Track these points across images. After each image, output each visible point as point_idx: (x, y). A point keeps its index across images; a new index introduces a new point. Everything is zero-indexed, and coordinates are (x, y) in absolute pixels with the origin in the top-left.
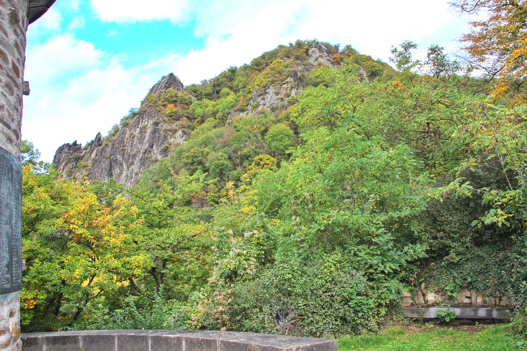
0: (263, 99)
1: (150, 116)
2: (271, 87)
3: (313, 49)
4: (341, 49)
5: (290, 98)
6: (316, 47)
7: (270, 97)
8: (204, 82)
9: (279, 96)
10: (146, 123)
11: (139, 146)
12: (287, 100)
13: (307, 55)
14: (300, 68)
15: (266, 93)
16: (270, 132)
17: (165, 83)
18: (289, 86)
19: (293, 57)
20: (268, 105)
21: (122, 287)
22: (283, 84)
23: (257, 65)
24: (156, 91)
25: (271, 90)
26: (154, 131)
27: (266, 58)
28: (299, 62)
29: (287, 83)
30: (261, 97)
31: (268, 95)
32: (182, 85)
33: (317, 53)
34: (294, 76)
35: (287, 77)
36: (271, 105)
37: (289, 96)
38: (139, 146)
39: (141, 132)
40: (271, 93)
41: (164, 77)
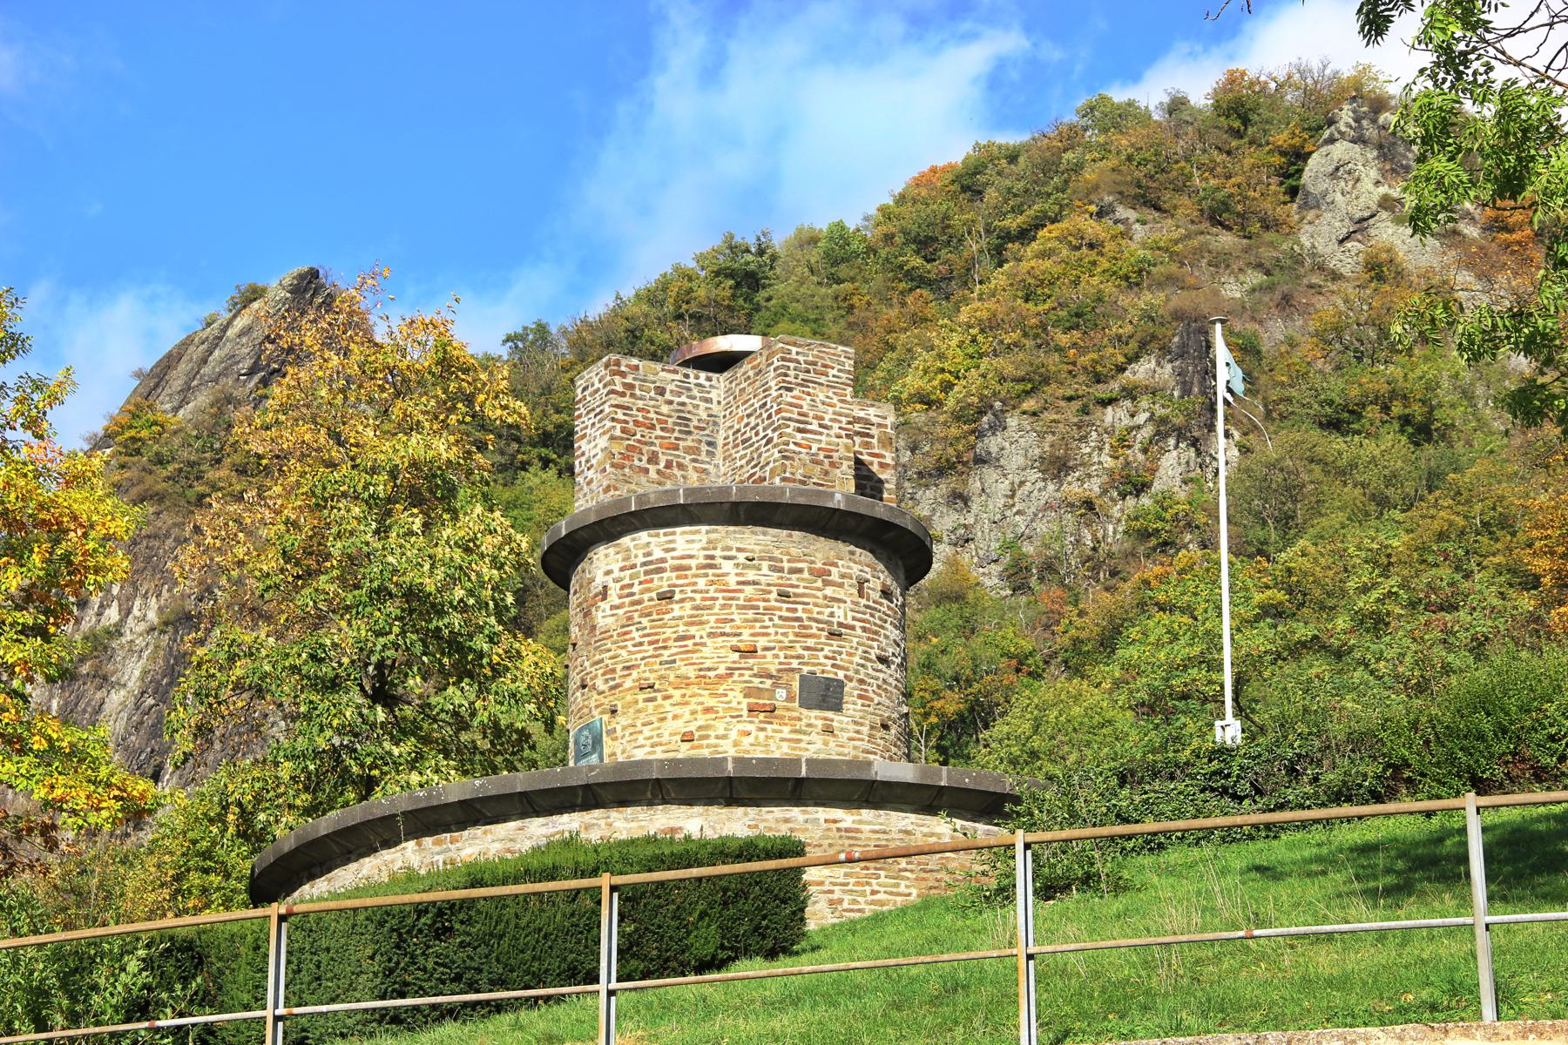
0: (960, 499)
2: (1012, 421)
3: (1341, 150)
5: (1146, 501)
6: (1360, 140)
7: (1004, 486)
9: (1073, 488)
10: (113, 614)
12: (1122, 509)
13: (1293, 192)
14: (1232, 290)
15: (980, 461)
16: (1010, 726)
17: (258, 334)
18: (1142, 418)
19: (1186, 206)
20: (988, 541)
21: (1527, 337)
22: (1105, 403)
23: (925, 244)
24: (186, 393)
25: (1016, 442)
27: (991, 195)
28: (1226, 240)
29: (1131, 393)
30: (944, 487)
31: (990, 474)
33: (1367, 184)
34: (1182, 354)
35: (1135, 358)
36: (1007, 546)
37: (1140, 488)
40: (1014, 460)
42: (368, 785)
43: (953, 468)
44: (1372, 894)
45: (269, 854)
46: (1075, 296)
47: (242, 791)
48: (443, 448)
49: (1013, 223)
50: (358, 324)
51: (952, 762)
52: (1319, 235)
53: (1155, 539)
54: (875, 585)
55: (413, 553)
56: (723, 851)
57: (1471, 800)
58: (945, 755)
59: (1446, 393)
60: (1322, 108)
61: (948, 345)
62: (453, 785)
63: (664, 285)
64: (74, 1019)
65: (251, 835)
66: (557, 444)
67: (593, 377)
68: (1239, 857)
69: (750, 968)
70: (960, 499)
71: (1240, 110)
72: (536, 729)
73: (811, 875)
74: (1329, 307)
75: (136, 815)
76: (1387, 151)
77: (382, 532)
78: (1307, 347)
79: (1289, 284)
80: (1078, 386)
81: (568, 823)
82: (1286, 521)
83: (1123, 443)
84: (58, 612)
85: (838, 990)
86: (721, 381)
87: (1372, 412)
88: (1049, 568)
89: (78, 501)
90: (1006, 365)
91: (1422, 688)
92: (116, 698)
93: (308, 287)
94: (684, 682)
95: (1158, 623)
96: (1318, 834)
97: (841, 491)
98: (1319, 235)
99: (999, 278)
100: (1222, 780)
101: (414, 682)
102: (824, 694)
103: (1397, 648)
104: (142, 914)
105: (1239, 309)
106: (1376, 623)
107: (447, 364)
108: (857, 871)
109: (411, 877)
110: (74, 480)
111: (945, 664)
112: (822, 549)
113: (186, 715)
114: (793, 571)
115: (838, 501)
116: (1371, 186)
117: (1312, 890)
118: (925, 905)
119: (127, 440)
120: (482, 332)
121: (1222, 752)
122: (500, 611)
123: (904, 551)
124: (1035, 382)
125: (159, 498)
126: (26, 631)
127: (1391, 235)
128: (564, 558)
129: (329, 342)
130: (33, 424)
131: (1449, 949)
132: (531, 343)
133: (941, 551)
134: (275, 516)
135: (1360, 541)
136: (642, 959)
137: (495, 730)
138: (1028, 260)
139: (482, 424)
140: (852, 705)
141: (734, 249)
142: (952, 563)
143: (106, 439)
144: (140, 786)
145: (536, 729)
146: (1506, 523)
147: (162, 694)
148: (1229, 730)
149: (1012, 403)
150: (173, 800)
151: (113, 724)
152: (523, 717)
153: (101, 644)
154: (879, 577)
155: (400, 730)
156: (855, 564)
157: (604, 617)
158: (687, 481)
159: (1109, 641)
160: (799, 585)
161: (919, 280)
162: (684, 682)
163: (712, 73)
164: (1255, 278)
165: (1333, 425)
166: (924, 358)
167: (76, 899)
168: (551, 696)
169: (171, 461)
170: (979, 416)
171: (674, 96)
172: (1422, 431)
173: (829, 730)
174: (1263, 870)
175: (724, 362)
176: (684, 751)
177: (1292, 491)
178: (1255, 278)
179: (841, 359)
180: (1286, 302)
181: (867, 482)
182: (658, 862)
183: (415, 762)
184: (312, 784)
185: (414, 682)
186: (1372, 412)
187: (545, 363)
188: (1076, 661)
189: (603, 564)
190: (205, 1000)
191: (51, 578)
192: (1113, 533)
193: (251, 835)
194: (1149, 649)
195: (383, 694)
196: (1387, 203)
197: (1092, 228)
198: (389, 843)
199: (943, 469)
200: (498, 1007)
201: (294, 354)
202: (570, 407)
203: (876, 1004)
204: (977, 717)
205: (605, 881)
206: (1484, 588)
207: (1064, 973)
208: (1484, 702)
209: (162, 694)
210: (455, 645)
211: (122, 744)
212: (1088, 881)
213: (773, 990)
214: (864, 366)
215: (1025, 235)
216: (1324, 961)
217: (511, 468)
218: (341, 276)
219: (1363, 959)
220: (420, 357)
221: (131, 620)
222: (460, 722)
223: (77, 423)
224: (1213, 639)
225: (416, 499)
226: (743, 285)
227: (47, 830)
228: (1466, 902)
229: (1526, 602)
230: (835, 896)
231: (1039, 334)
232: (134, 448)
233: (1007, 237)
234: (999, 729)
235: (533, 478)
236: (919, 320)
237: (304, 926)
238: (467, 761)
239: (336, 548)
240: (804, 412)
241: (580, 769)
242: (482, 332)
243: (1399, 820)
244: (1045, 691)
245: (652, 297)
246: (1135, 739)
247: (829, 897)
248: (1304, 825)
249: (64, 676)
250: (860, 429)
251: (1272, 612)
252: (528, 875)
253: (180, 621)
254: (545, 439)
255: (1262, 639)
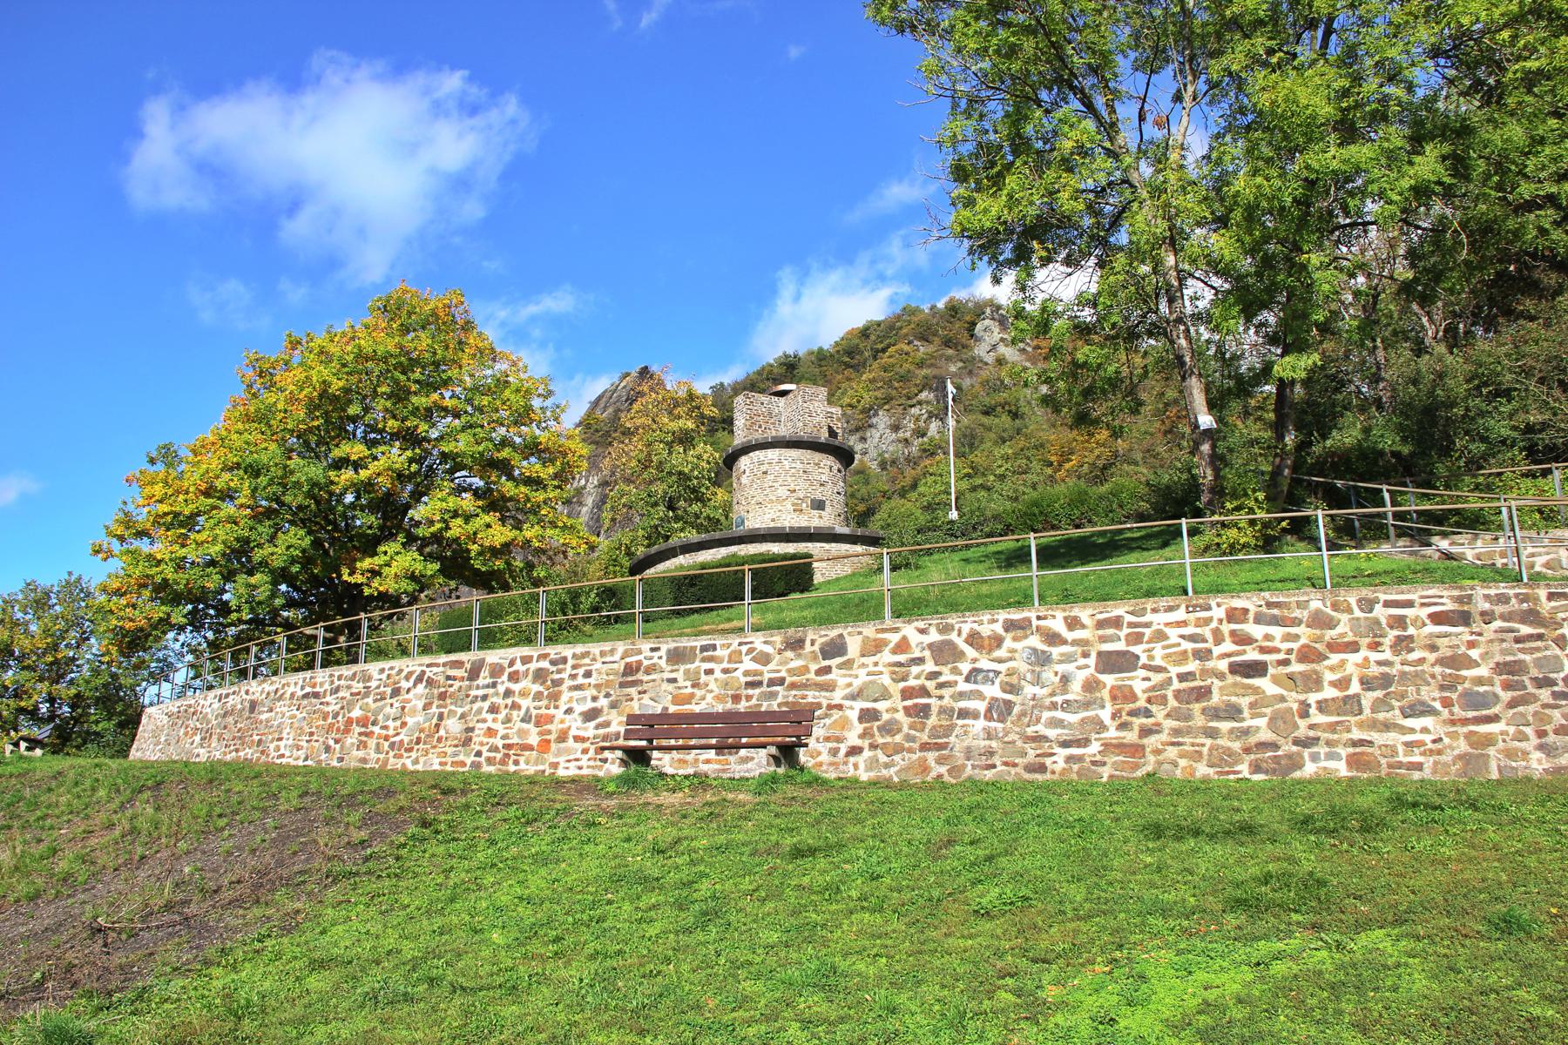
0: (863, 439)
3: (987, 322)
9: (901, 435)
10: (583, 482)
14: (953, 369)
20: (873, 453)
25: (882, 420)
27: (873, 337)
28: (950, 352)
29: (920, 403)
30: (858, 435)
31: (874, 431)
37: (923, 435)
40: (881, 426)
42: (667, 538)
43: (861, 429)
44: (1000, 567)
45: (635, 560)
46: (902, 371)
47: (626, 541)
48: (690, 425)
49: (880, 346)
50: (661, 383)
51: (862, 525)
52: (981, 350)
53: (929, 452)
54: (835, 468)
55: (680, 459)
56: (785, 557)
57: (1032, 535)
58: (859, 524)
59: (1022, 403)
60: (979, 310)
61: (860, 389)
62: (692, 536)
63: (763, 368)
64: (575, 612)
65: (629, 554)
66: (728, 423)
67: (740, 399)
68: (957, 556)
69: (796, 596)
70: (863, 439)
71: (954, 310)
72: (723, 519)
73: (815, 565)
74: (985, 374)
75: (592, 548)
76: (1002, 322)
77: (670, 453)
78: (977, 386)
79: (971, 366)
80: (902, 401)
81: (733, 549)
82: (971, 446)
83: (917, 420)
84: (566, 481)
85: (825, 602)
86: (782, 400)
87: (999, 409)
88: (893, 462)
89: (571, 444)
90: (879, 394)
91: (1016, 499)
92: (585, 509)
93: (644, 372)
94: (771, 501)
95: (930, 479)
96: (982, 548)
97: (824, 436)
98: (981, 350)
99: (875, 365)
100: (952, 531)
101: (682, 503)
102: (819, 505)
103: (1007, 488)
104: (595, 578)
105: (954, 375)
106: (1002, 477)
107: (691, 396)
108: (832, 566)
109: (682, 567)
110: (570, 437)
111: (859, 495)
112: (817, 456)
113: (607, 515)
115: (823, 440)
116: (997, 335)
117: (981, 567)
118: (854, 574)
119: (586, 424)
120: (703, 387)
121: (952, 522)
122: (709, 479)
123: (844, 456)
124: (888, 400)
125: (597, 443)
126: (556, 487)
127: (1002, 349)
128: (731, 460)
129: (652, 389)
130: (556, 419)
131: (1024, 584)
132: (719, 390)
133: (857, 457)
134: (636, 447)
135: (999, 451)
136: (761, 592)
137: (708, 518)
138: (885, 359)
139: (702, 416)
140: (828, 509)
141: (787, 356)
142: (861, 461)
143: (578, 425)
144: (593, 538)
145: (723, 519)
146: (1042, 445)
147: (600, 509)
148: (954, 515)
149: (880, 407)
150: (603, 543)
151: (584, 518)
152: (719, 514)
153: (579, 492)
154: (837, 466)
155: (677, 519)
156: (828, 461)
157: (744, 480)
158: (771, 434)
159: (914, 486)
160: (810, 468)
161: (848, 366)
162: (771, 501)
163: (797, 298)
164: (960, 364)
165: (986, 413)
166: (850, 392)
167: (574, 574)
168: (727, 508)
169: (602, 430)
170: (869, 412)
171: (784, 307)
172: (1015, 415)
174: (966, 561)
175: (783, 394)
176: (772, 525)
177: (973, 437)
178: (960, 364)
179: (823, 392)
180: (970, 372)
181: (832, 433)
182: (764, 561)
183: (682, 530)
184: (649, 538)
185: (682, 503)
186: (999, 409)
187: (724, 398)
188: (903, 493)
189: (744, 462)
190: (615, 607)
191: (563, 470)
192: (914, 450)
193: (629, 554)
194: (927, 489)
195: (671, 507)
196: (1002, 340)
197: (906, 348)
198: (675, 556)
199: (858, 429)
200: (711, 609)
201: (641, 394)
202: (731, 410)
203: (837, 606)
204: (870, 512)
205: (746, 567)
206: (1036, 466)
207: (899, 595)
208: (1036, 504)
209: (600, 509)
210: (694, 490)
211: (587, 524)
212: (907, 565)
213: (803, 603)
214: (831, 395)
215: (884, 350)
216: (985, 589)
217: (712, 431)
218: (654, 368)
219: (996, 588)
220: (682, 394)
221: (590, 484)
222: (697, 516)
223: (572, 418)
224: (948, 484)
225: (681, 442)
226: (790, 368)
227: (564, 553)
228: (1030, 569)
229: (1049, 471)
231: (889, 383)
232: (588, 426)
233: (878, 351)
234: (877, 517)
235: (719, 434)
236: (849, 379)
237: (647, 583)
238: (699, 528)
239: (655, 459)
240: (808, 409)
241: (737, 531)
242: (703, 387)
243: (1007, 543)
244: (893, 503)
245: (759, 373)
246: (922, 518)
247: (822, 572)
248: (978, 545)
249: (567, 502)
250: (830, 416)
251: (969, 476)
252: (721, 566)
253: (604, 484)
254: (724, 421)
255: (965, 485)
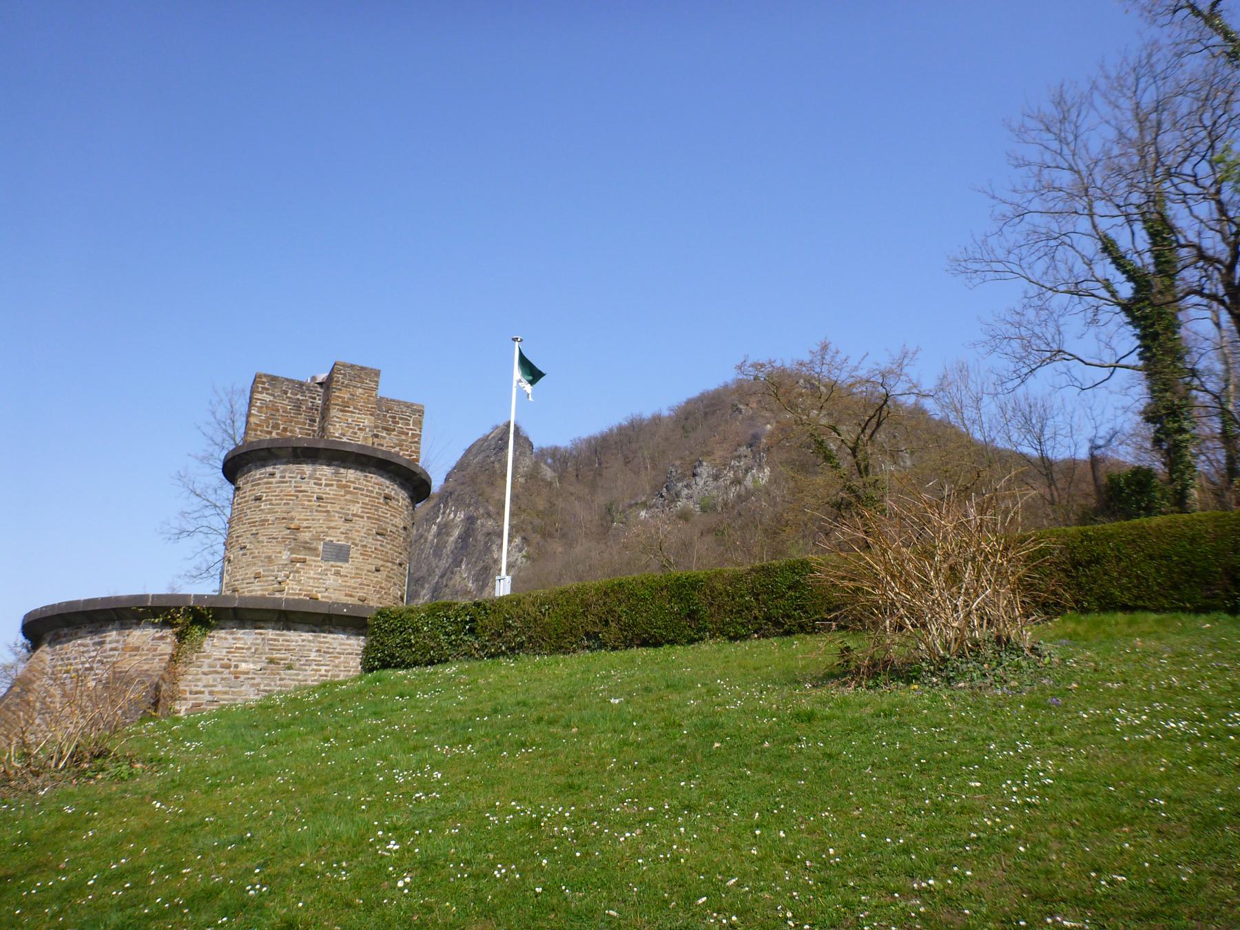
0: (688, 486)
1: (460, 503)
4: (1138, 331)
8: (611, 430)
10: (452, 516)
11: (434, 562)
26: (465, 537)
32: (531, 445)
38: (434, 562)
39: (439, 534)
41: (497, 427)
114: (327, 485)
173: (337, 573)
230: (256, 681)
